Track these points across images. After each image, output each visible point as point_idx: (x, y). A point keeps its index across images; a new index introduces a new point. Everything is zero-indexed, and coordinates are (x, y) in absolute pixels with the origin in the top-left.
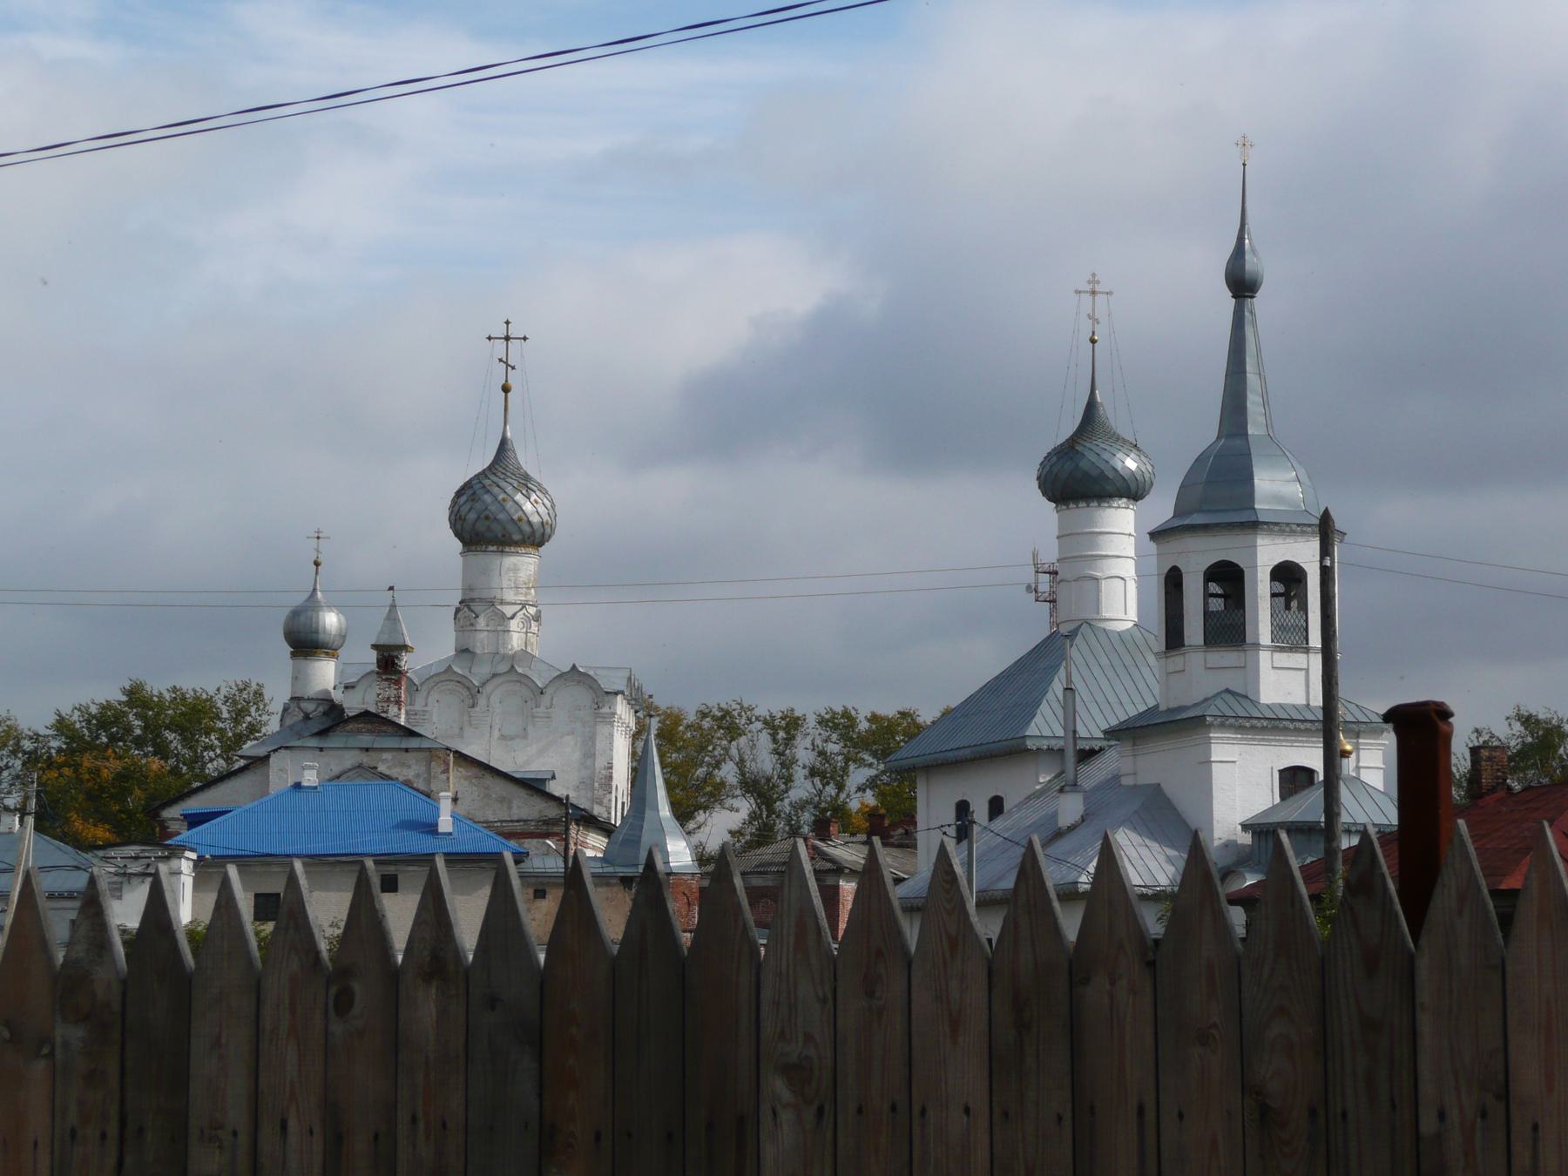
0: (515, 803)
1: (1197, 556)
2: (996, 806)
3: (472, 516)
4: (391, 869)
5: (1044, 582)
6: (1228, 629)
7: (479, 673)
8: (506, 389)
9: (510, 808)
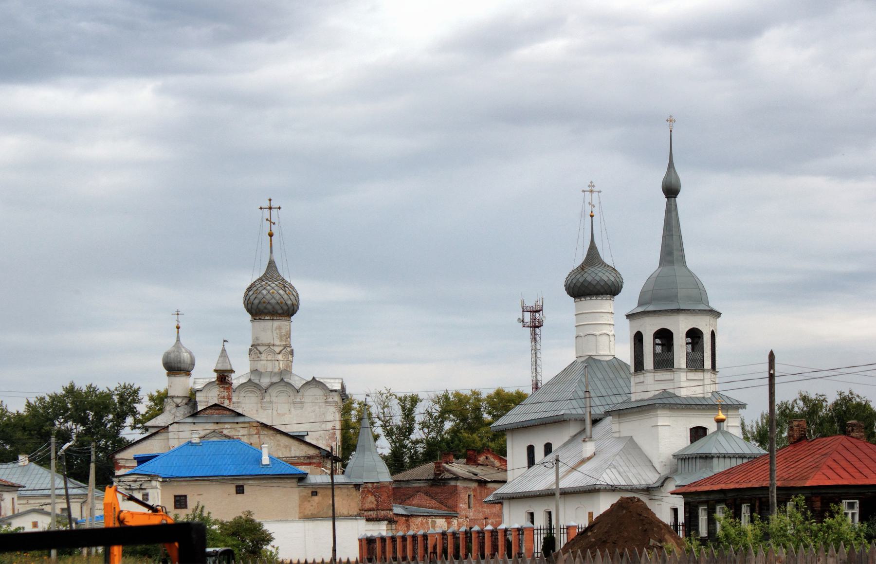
0: (293, 449)
1: (649, 327)
2: (548, 449)
3: (256, 301)
4: (241, 483)
5: (528, 317)
6: (664, 362)
7: (265, 381)
8: (271, 235)
9: (290, 451)
